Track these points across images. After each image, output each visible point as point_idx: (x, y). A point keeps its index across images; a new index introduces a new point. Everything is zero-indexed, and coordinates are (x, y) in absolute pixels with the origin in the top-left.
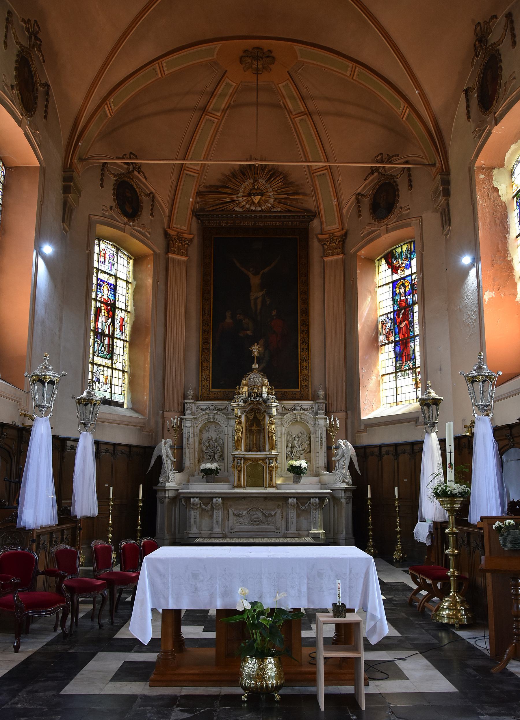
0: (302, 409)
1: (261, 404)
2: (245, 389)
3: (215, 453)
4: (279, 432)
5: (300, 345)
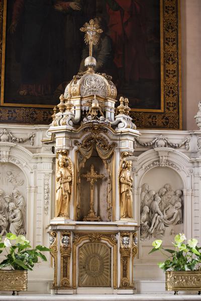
0: (168, 144)
1: (106, 131)
2: (76, 102)
5: (164, 33)
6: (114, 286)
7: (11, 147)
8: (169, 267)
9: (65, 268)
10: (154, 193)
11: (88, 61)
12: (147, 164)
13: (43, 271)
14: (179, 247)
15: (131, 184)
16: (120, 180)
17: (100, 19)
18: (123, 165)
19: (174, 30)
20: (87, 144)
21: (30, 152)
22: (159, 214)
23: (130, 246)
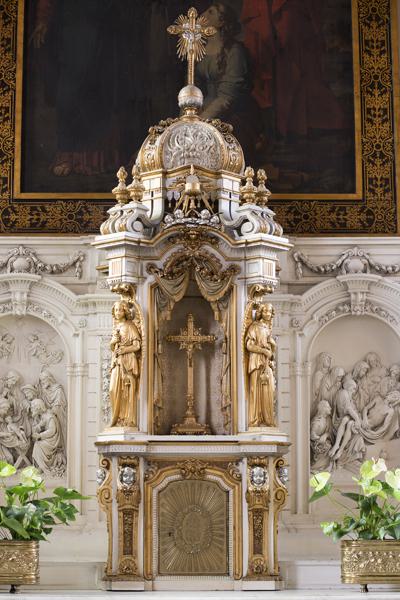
0: (370, 267)
1: (215, 241)
2: (152, 182)
3: (32, 441)
4: (283, 357)
5: (361, 31)
6: (235, 574)
7: (33, 284)
8: (346, 533)
9: (128, 537)
10: (341, 373)
11: (184, 96)
12: (323, 311)
13: (85, 541)
14: (369, 490)
15: (269, 353)
16: (245, 344)
17: (222, 8)
18: (254, 312)
19: (383, 24)
20: (175, 270)
21: (70, 292)
22: (352, 419)
23: (266, 487)
